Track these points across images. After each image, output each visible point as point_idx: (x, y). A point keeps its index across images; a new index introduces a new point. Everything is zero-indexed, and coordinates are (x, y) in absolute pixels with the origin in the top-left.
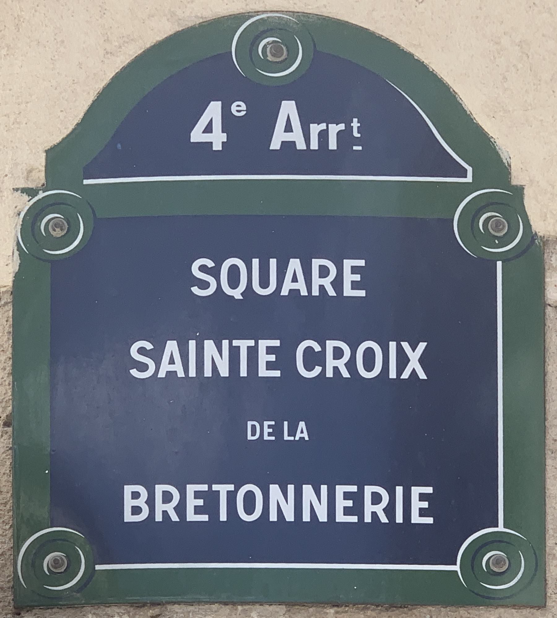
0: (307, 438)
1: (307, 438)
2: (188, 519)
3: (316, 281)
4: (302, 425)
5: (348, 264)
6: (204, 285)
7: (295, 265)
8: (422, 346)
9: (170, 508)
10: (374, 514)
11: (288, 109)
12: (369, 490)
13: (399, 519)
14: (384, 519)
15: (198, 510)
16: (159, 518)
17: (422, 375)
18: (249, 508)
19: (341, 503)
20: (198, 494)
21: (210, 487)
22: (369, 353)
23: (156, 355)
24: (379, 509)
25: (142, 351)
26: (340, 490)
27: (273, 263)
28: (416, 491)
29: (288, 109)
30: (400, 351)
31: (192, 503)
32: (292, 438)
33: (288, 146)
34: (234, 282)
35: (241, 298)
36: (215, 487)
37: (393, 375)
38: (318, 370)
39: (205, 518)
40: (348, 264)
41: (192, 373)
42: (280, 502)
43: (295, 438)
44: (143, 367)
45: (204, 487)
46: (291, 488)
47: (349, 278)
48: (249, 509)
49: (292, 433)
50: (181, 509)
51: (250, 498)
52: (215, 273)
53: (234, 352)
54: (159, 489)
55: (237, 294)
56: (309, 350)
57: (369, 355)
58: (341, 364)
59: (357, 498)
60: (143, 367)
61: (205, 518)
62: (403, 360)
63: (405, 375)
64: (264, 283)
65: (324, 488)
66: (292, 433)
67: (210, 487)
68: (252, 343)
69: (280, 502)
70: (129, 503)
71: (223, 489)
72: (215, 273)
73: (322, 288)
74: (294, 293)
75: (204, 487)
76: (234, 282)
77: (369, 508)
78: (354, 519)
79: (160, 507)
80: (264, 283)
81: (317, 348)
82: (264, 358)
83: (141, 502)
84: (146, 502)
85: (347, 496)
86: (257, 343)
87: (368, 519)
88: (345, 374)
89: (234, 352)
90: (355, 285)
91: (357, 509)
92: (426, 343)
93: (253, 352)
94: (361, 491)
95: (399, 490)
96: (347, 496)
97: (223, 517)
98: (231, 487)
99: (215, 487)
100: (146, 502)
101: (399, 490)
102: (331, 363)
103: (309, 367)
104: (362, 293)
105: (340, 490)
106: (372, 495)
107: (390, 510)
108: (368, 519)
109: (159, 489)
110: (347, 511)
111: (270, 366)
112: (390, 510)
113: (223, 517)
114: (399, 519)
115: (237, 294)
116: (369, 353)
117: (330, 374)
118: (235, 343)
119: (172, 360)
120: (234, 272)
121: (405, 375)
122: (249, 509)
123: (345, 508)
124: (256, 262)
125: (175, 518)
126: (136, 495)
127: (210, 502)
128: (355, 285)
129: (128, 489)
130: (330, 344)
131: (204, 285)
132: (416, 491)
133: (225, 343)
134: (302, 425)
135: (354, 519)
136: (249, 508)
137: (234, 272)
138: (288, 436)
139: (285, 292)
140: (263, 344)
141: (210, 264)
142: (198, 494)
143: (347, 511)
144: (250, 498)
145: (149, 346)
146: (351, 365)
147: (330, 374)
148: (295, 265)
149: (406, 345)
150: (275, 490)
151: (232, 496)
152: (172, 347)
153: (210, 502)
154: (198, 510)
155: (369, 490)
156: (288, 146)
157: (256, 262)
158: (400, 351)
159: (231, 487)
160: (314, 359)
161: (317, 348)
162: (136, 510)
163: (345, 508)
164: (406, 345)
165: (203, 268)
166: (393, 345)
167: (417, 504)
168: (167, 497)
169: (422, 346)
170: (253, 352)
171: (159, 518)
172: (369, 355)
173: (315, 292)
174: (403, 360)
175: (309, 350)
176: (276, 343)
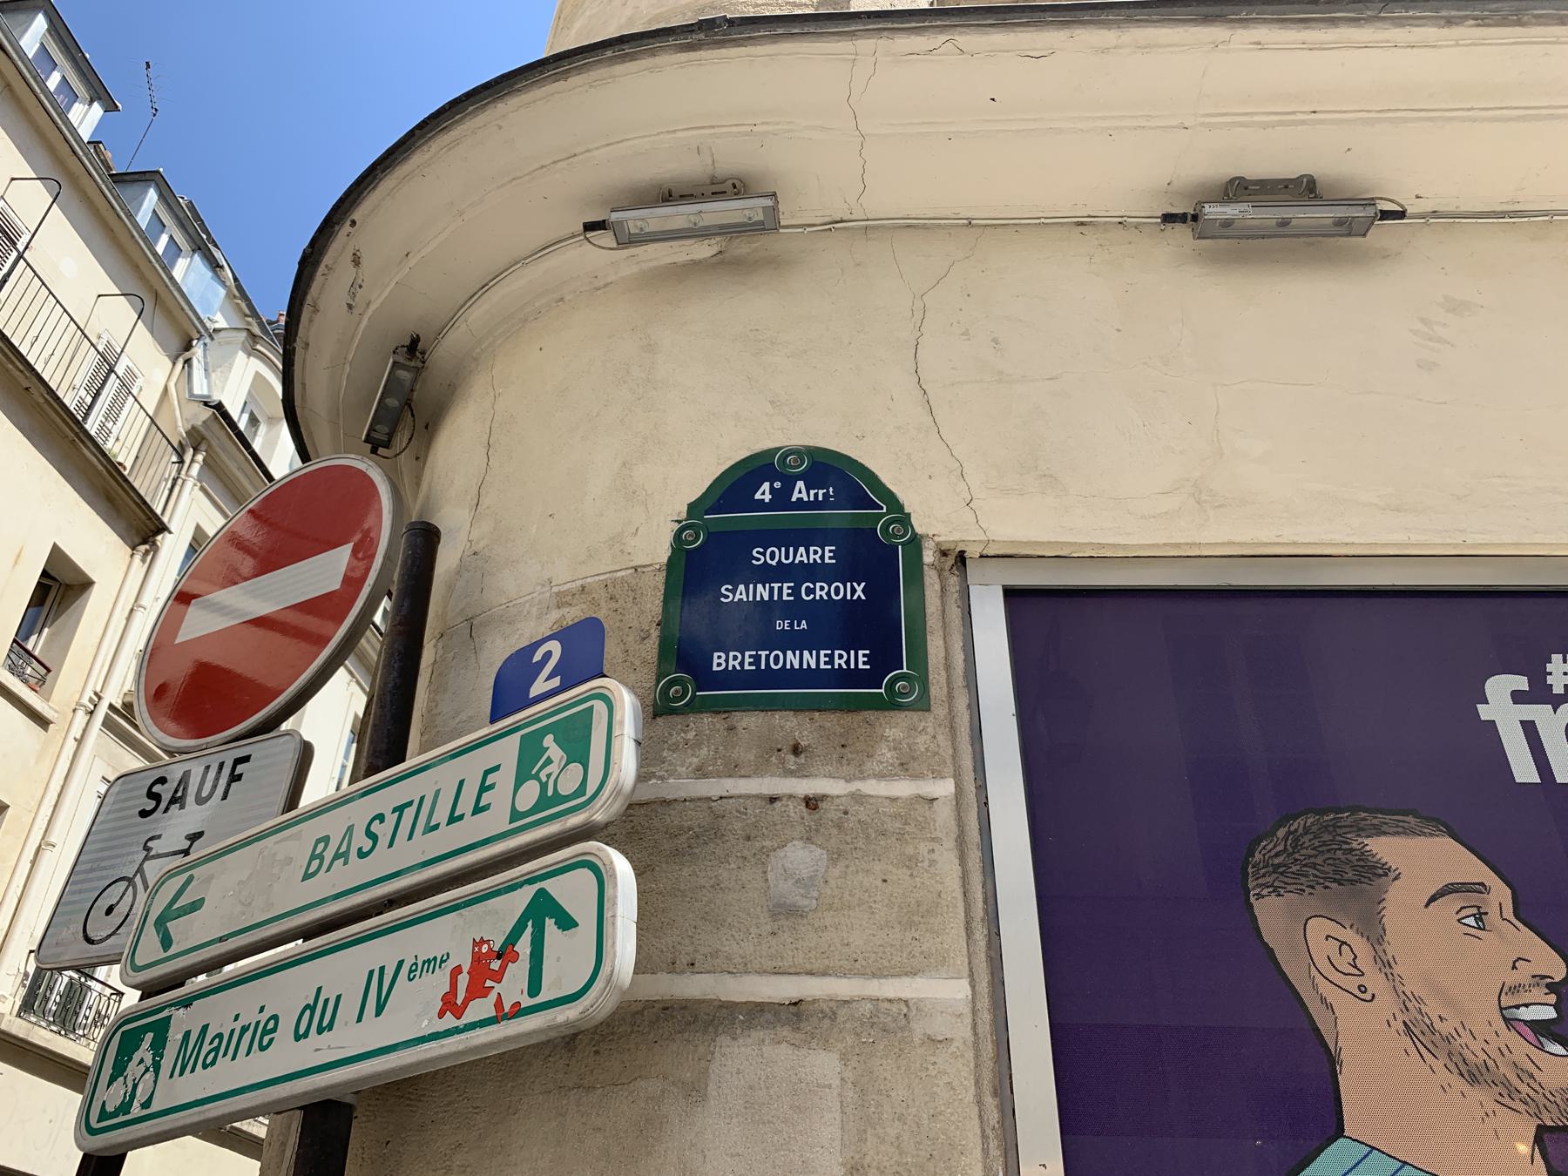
7: (802, 549)
11: (800, 484)
19: (823, 659)
23: (734, 592)
24: (842, 662)
26: (822, 653)
29: (800, 484)
31: (747, 660)
34: (772, 558)
42: (792, 659)
47: (827, 555)
52: (764, 554)
53: (772, 589)
57: (837, 589)
58: (823, 593)
59: (831, 657)
64: (787, 558)
69: (792, 659)
70: (716, 661)
71: (763, 653)
72: (764, 554)
76: (772, 558)
77: (837, 661)
79: (731, 663)
80: (787, 558)
82: (786, 591)
89: (772, 589)
91: (831, 662)
93: (781, 589)
102: (818, 593)
105: (822, 653)
144: (777, 657)
146: (828, 594)
148: (802, 549)
151: (768, 657)
160: (810, 591)
170: (781, 589)
172: (837, 589)
174: (854, 591)
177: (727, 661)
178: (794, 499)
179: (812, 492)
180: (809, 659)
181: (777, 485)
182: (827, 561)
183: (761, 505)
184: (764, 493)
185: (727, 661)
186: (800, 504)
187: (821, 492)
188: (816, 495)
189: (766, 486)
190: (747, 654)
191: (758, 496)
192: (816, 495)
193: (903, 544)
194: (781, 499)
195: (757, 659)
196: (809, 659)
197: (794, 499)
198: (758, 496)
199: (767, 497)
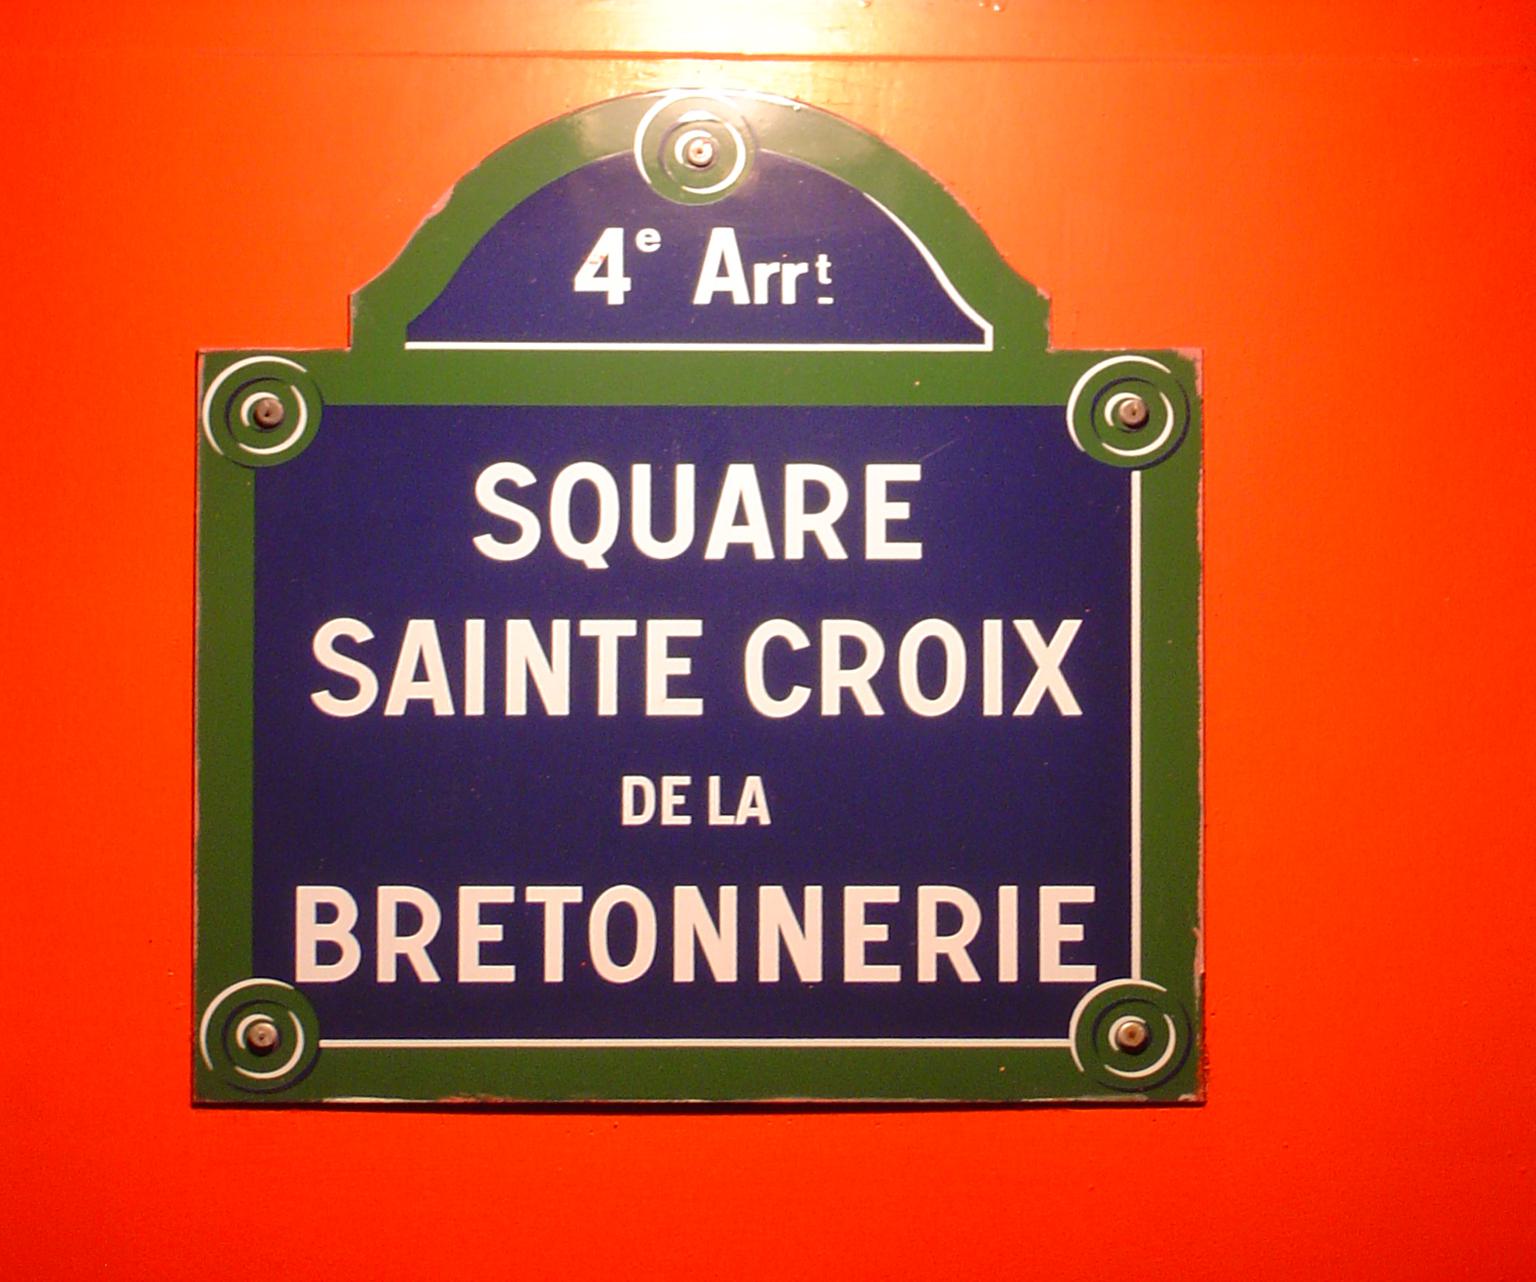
0: (765, 820)
1: (765, 820)
2: (463, 978)
3: (797, 522)
4: (753, 785)
5: (878, 476)
6: (508, 532)
7: (741, 479)
8: (1069, 629)
9: (415, 948)
10: (943, 961)
11: (723, 242)
12: (930, 897)
13: (1008, 972)
14: (968, 973)
15: (489, 954)
16: (387, 973)
17: (1069, 706)
18: (622, 947)
19: (858, 933)
20: (488, 913)
21: (520, 894)
22: (932, 651)
23: (381, 656)
24: (955, 947)
25: (343, 645)
26: (857, 897)
27: (685, 476)
28: (1052, 897)
29: (723, 242)
30: (1014, 647)
31: (473, 933)
32: (728, 820)
33: (722, 299)
34: (584, 521)
35: (604, 565)
36: (534, 894)
37: (993, 706)
38: (799, 696)
39: (505, 974)
40: (878, 476)
41: (475, 706)
42: (702, 931)
43: (735, 819)
44: (345, 688)
45: (504, 894)
46: (728, 895)
47: (881, 511)
48: (622, 950)
49: (729, 805)
50: (444, 950)
51: (622, 921)
52: (536, 499)
53: (584, 653)
54: (389, 897)
55: (593, 555)
56: (777, 646)
57: (932, 656)
58: (860, 681)
59: (900, 919)
60: (345, 688)
61: (505, 974)
62: (1019, 668)
63: (1027, 706)
64: (663, 527)
65: (813, 895)
66: (729, 805)
67: (520, 894)
68: (628, 627)
69: (702, 931)
70: (308, 933)
71: (554, 899)
72: (536, 499)
73: (810, 539)
74: (740, 553)
75: (504, 894)
76: (584, 521)
77: (930, 945)
78: (891, 974)
79: (390, 944)
80: (663, 527)
81: (798, 640)
82: (661, 667)
83: (340, 931)
84: (353, 931)
85: (874, 914)
86: (642, 629)
87: (927, 973)
88: (871, 706)
89: (584, 653)
90: (896, 531)
91: (900, 947)
92: (1078, 623)
93: (632, 653)
94: (909, 901)
95: (1008, 896)
96: (874, 914)
97: (554, 970)
98: (575, 894)
99: (534, 894)
100: (353, 931)
101: (1008, 896)
102: (833, 677)
103: (777, 688)
104: (912, 551)
105: (857, 897)
106: (938, 911)
107: (984, 950)
108: (927, 973)
109: (389, 897)
110: (874, 954)
111: (677, 687)
112: (984, 950)
113: (554, 970)
114: (1008, 972)
115: (593, 555)
116: (932, 651)
117: (831, 706)
118: (588, 627)
119: (422, 674)
120: (585, 501)
121: (1027, 706)
122: (622, 950)
123: (868, 945)
124: (642, 474)
125: (427, 973)
126: (326, 913)
127: (520, 931)
128: (896, 531)
129: (308, 897)
130: (834, 630)
131: (508, 532)
132: (1052, 897)
133: (560, 628)
134: (753, 785)
135: (891, 974)
136: (622, 947)
137: (585, 501)
138: (722, 814)
139: (715, 551)
140: (660, 630)
141: (523, 476)
142: (488, 913)
143: (874, 954)
144: (622, 921)
145: (361, 632)
146: (886, 683)
147: (831, 706)
148: (741, 479)
149: (1027, 629)
150: (687, 899)
151: (576, 918)
152: (421, 636)
153: (520, 931)
154: (489, 954)
155: (930, 897)
156: (722, 299)
157: (642, 474)
158: (1014, 647)
159: (575, 894)
160: (788, 668)
161: (798, 640)
162: (328, 953)
163: (868, 945)
164: (1027, 629)
165: (505, 489)
166: (993, 629)
167: (1054, 933)
168: (408, 919)
169: (1069, 629)
170: (632, 653)
171: (387, 973)
172: (932, 656)
173: (794, 550)
174: (1019, 668)
175: (777, 646)
176: (692, 628)
177: (366, 931)
178: (702, 296)
179: (763, 271)
180: (790, 932)
181: (649, 240)
182: (878, 547)
183: (594, 317)
184: (604, 271)
185: (366, 931)
186: (725, 319)
187: (792, 272)
188: (775, 282)
189: (610, 243)
190: (471, 897)
191: (585, 281)
192: (775, 282)
193: (1144, 465)
194: (662, 295)
195: (522, 923)
196: (790, 932)
197: (702, 296)
198: (585, 281)
199: (616, 288)
